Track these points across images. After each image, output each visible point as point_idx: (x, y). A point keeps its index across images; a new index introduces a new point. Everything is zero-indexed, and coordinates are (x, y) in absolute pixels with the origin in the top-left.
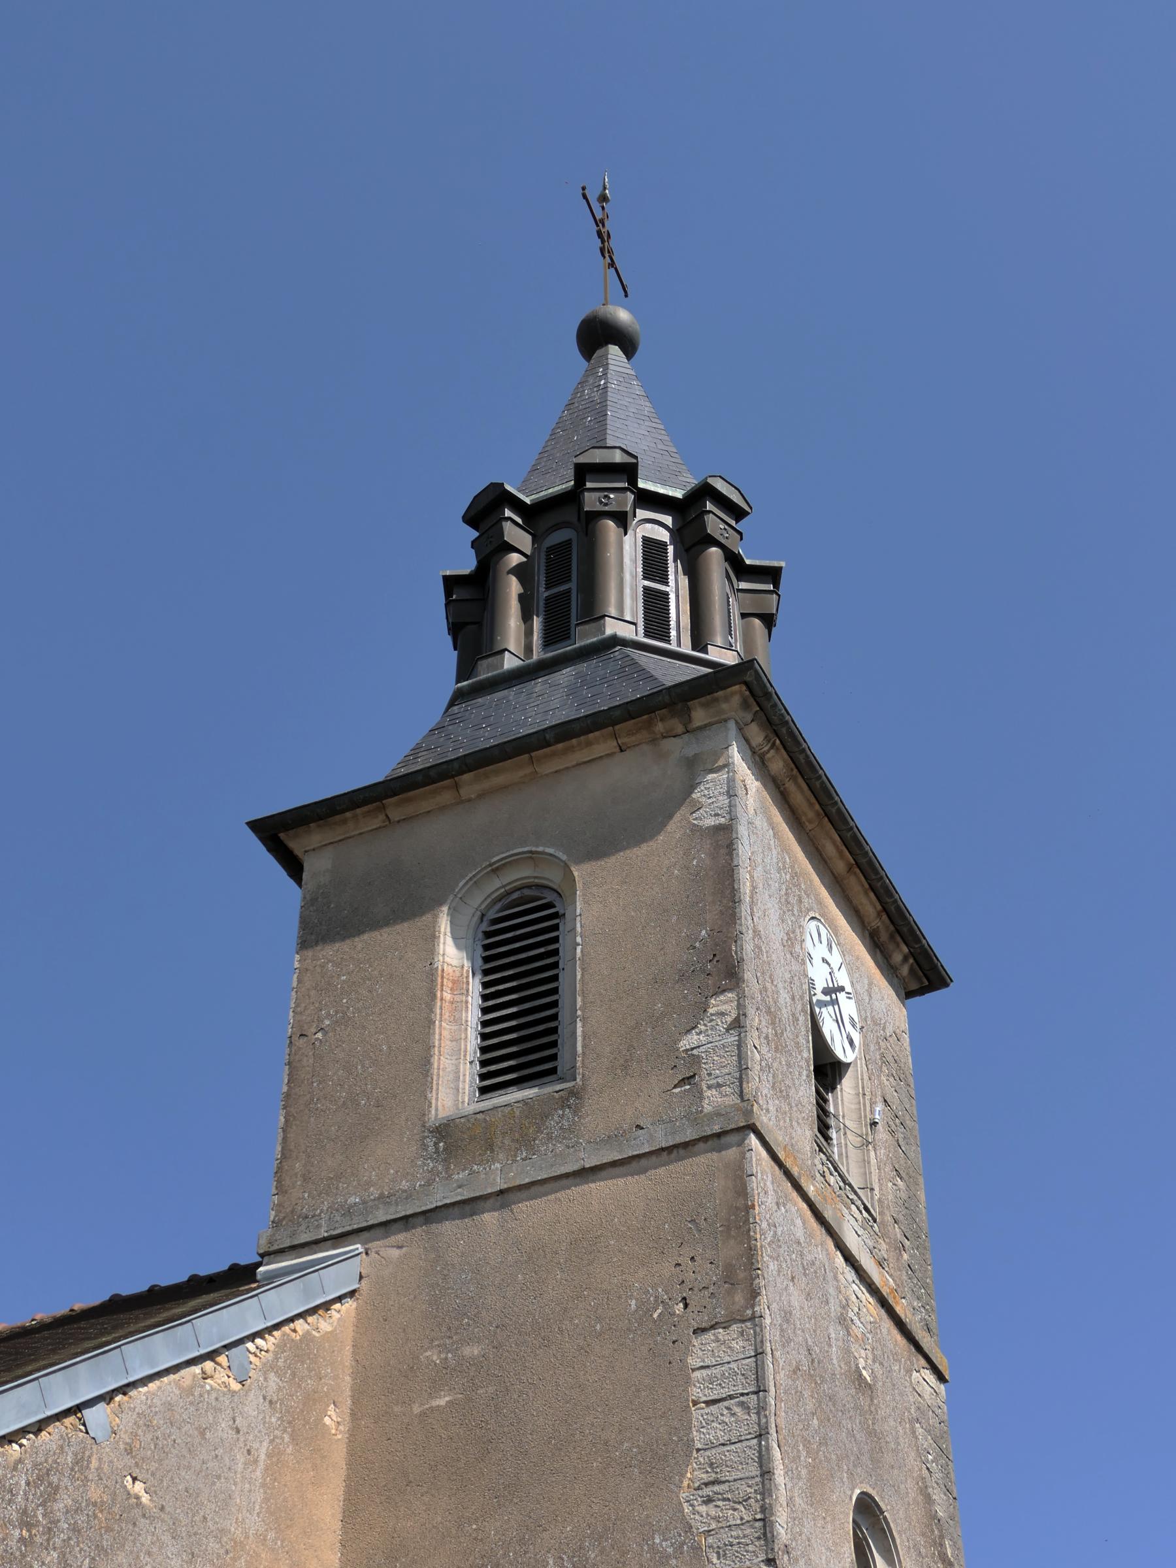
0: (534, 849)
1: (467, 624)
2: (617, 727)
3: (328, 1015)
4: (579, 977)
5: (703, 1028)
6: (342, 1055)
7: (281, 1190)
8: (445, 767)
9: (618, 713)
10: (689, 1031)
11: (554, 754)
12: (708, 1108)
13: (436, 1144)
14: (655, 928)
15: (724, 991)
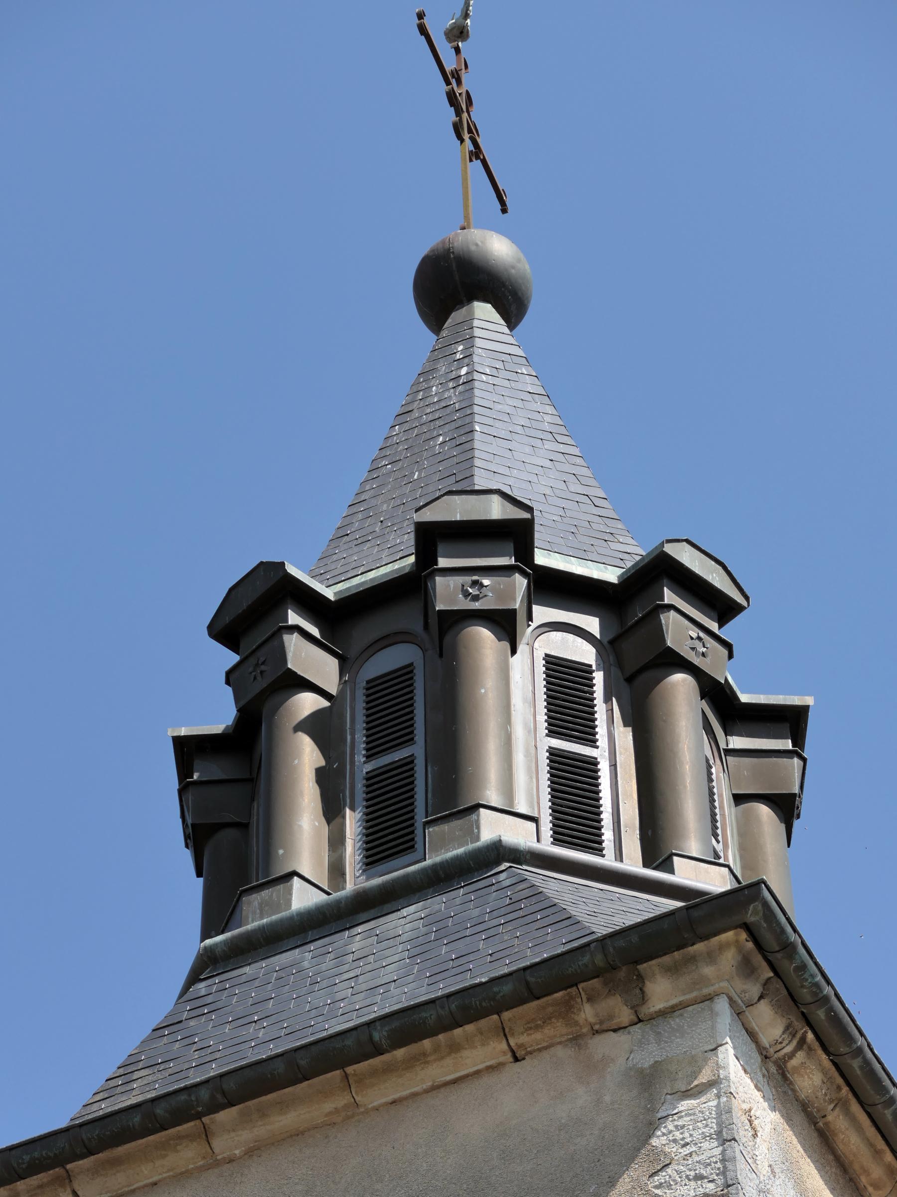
2: (506, 1015)
9: (507, 988)
11: (389, 1070)
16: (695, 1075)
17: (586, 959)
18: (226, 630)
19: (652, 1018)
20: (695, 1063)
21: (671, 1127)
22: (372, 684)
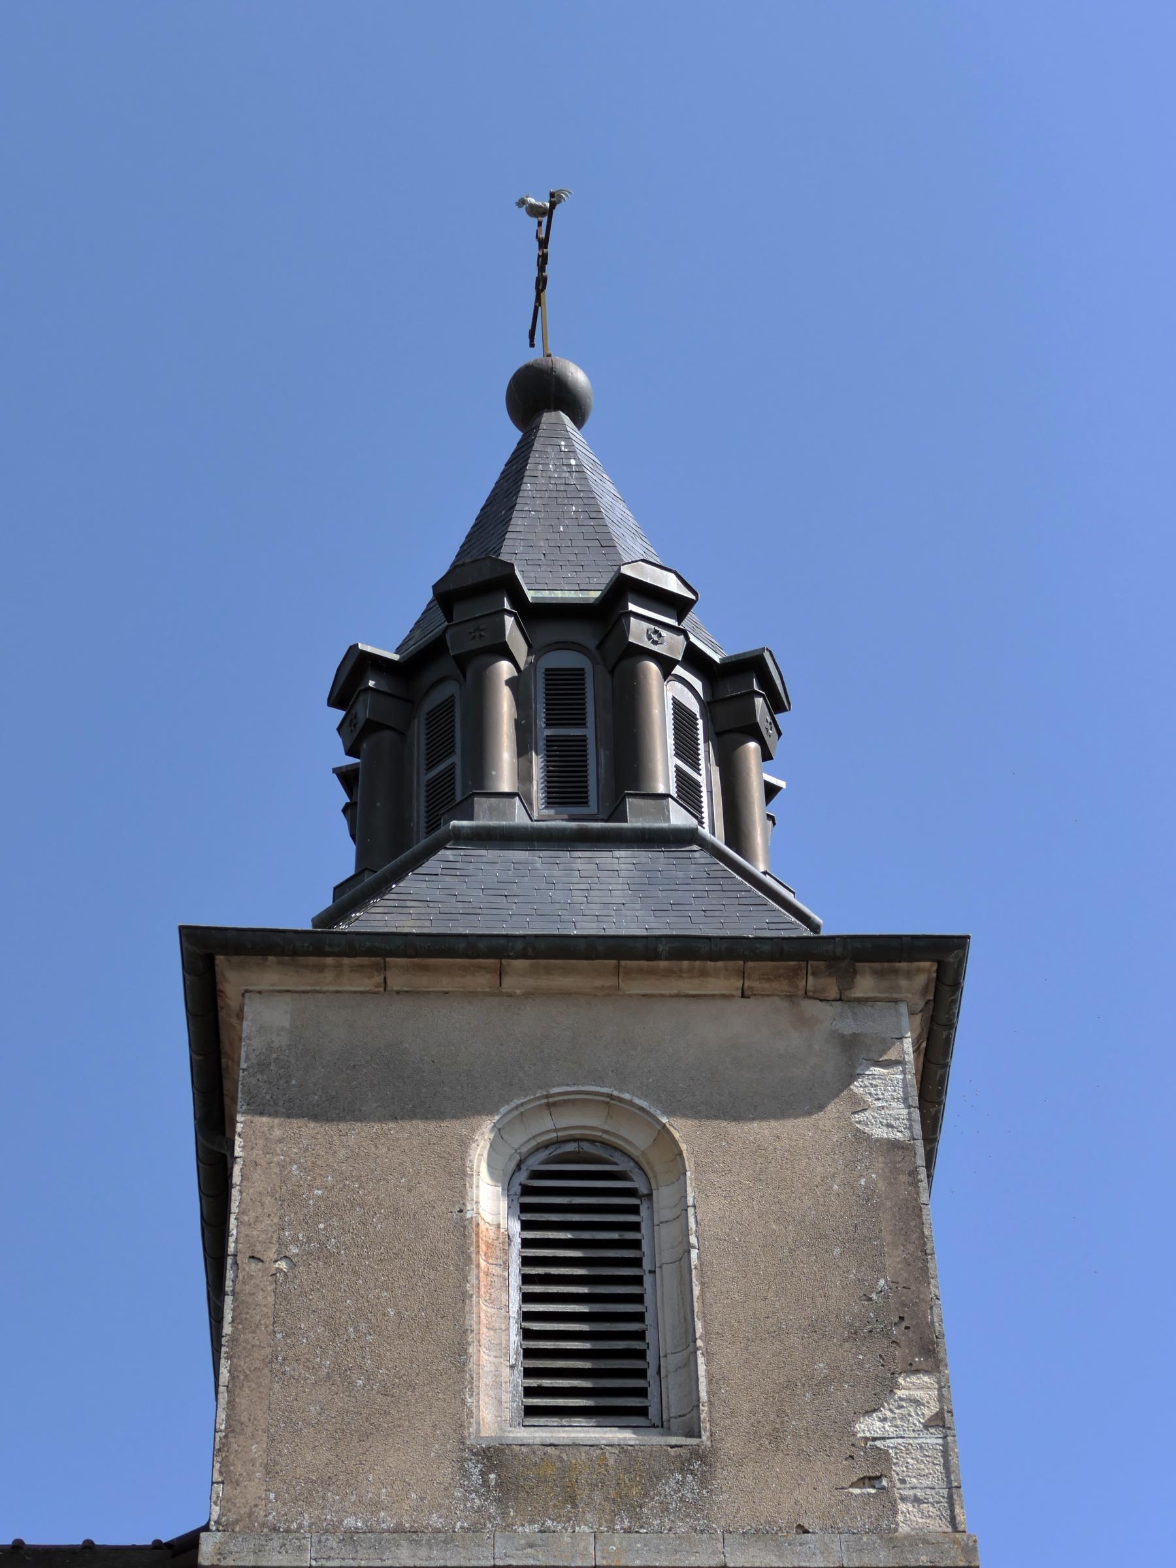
0: (616, 1093)
1: (389, 728)
2: (750, 964)
3: (295, 1240)
4: (696, 1291)
5: (888, 1414)
6: (322, 1305)
7: (227, 1477)
8: (502, 941)
9: (767, 948)
10: (868, 1413)
11: (651, 972)
12: (904, 1529)
13: (483, 1474)
14: (809, 1255)
15: (917, 1371)
16: (884, 1052)
17: (830, 947)
18: (336, 700)
19: (849, 1001)
20: (886, 1046)
21: (867, 1083)
22: (430, 714)
